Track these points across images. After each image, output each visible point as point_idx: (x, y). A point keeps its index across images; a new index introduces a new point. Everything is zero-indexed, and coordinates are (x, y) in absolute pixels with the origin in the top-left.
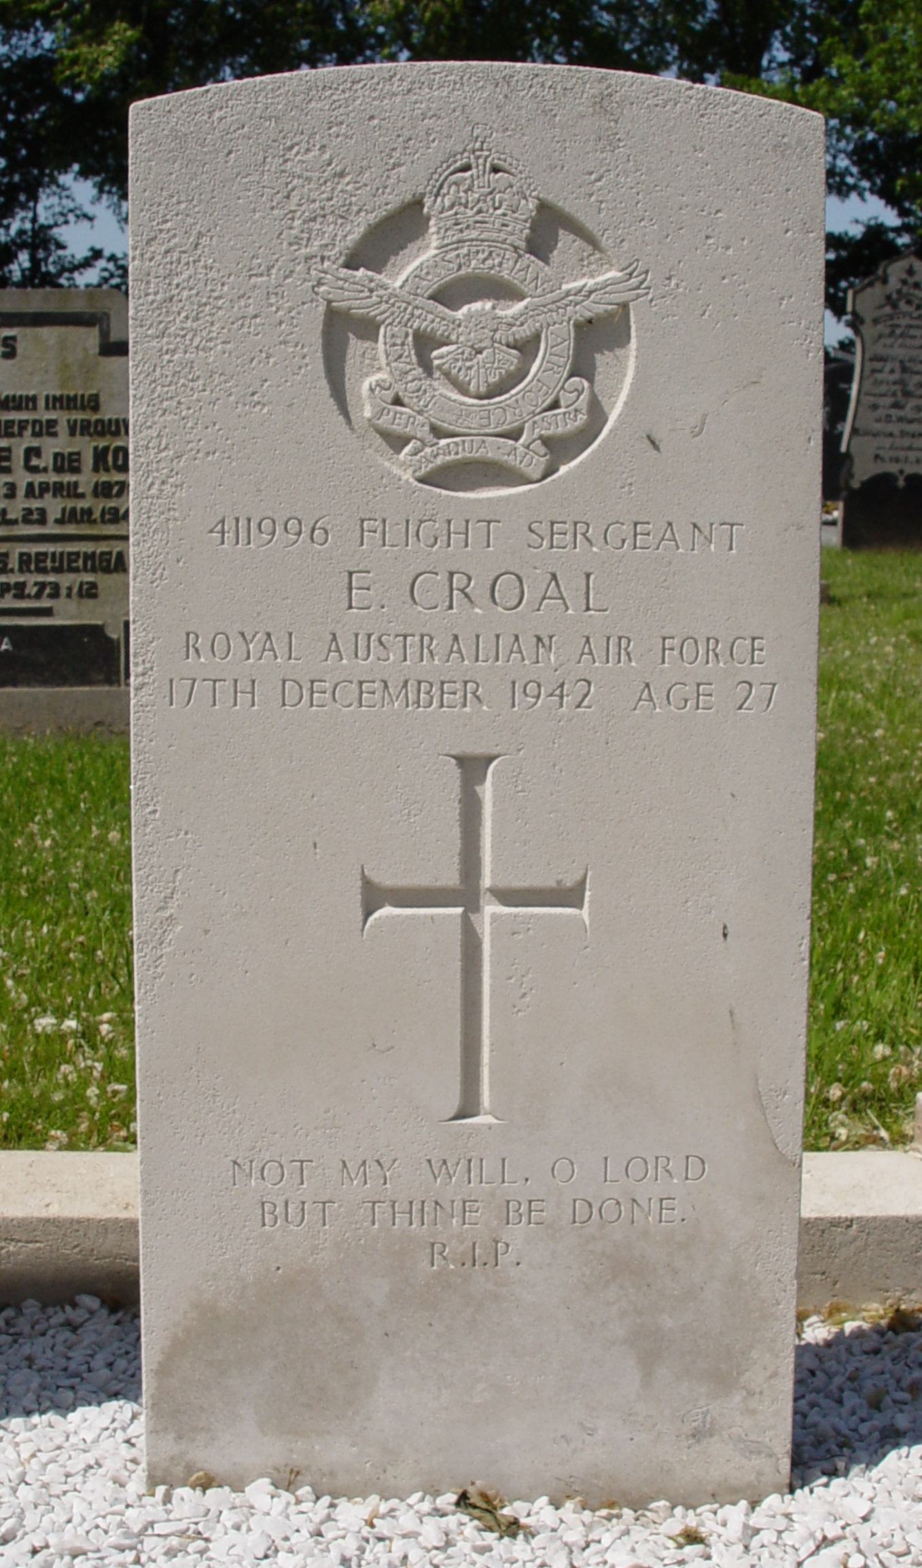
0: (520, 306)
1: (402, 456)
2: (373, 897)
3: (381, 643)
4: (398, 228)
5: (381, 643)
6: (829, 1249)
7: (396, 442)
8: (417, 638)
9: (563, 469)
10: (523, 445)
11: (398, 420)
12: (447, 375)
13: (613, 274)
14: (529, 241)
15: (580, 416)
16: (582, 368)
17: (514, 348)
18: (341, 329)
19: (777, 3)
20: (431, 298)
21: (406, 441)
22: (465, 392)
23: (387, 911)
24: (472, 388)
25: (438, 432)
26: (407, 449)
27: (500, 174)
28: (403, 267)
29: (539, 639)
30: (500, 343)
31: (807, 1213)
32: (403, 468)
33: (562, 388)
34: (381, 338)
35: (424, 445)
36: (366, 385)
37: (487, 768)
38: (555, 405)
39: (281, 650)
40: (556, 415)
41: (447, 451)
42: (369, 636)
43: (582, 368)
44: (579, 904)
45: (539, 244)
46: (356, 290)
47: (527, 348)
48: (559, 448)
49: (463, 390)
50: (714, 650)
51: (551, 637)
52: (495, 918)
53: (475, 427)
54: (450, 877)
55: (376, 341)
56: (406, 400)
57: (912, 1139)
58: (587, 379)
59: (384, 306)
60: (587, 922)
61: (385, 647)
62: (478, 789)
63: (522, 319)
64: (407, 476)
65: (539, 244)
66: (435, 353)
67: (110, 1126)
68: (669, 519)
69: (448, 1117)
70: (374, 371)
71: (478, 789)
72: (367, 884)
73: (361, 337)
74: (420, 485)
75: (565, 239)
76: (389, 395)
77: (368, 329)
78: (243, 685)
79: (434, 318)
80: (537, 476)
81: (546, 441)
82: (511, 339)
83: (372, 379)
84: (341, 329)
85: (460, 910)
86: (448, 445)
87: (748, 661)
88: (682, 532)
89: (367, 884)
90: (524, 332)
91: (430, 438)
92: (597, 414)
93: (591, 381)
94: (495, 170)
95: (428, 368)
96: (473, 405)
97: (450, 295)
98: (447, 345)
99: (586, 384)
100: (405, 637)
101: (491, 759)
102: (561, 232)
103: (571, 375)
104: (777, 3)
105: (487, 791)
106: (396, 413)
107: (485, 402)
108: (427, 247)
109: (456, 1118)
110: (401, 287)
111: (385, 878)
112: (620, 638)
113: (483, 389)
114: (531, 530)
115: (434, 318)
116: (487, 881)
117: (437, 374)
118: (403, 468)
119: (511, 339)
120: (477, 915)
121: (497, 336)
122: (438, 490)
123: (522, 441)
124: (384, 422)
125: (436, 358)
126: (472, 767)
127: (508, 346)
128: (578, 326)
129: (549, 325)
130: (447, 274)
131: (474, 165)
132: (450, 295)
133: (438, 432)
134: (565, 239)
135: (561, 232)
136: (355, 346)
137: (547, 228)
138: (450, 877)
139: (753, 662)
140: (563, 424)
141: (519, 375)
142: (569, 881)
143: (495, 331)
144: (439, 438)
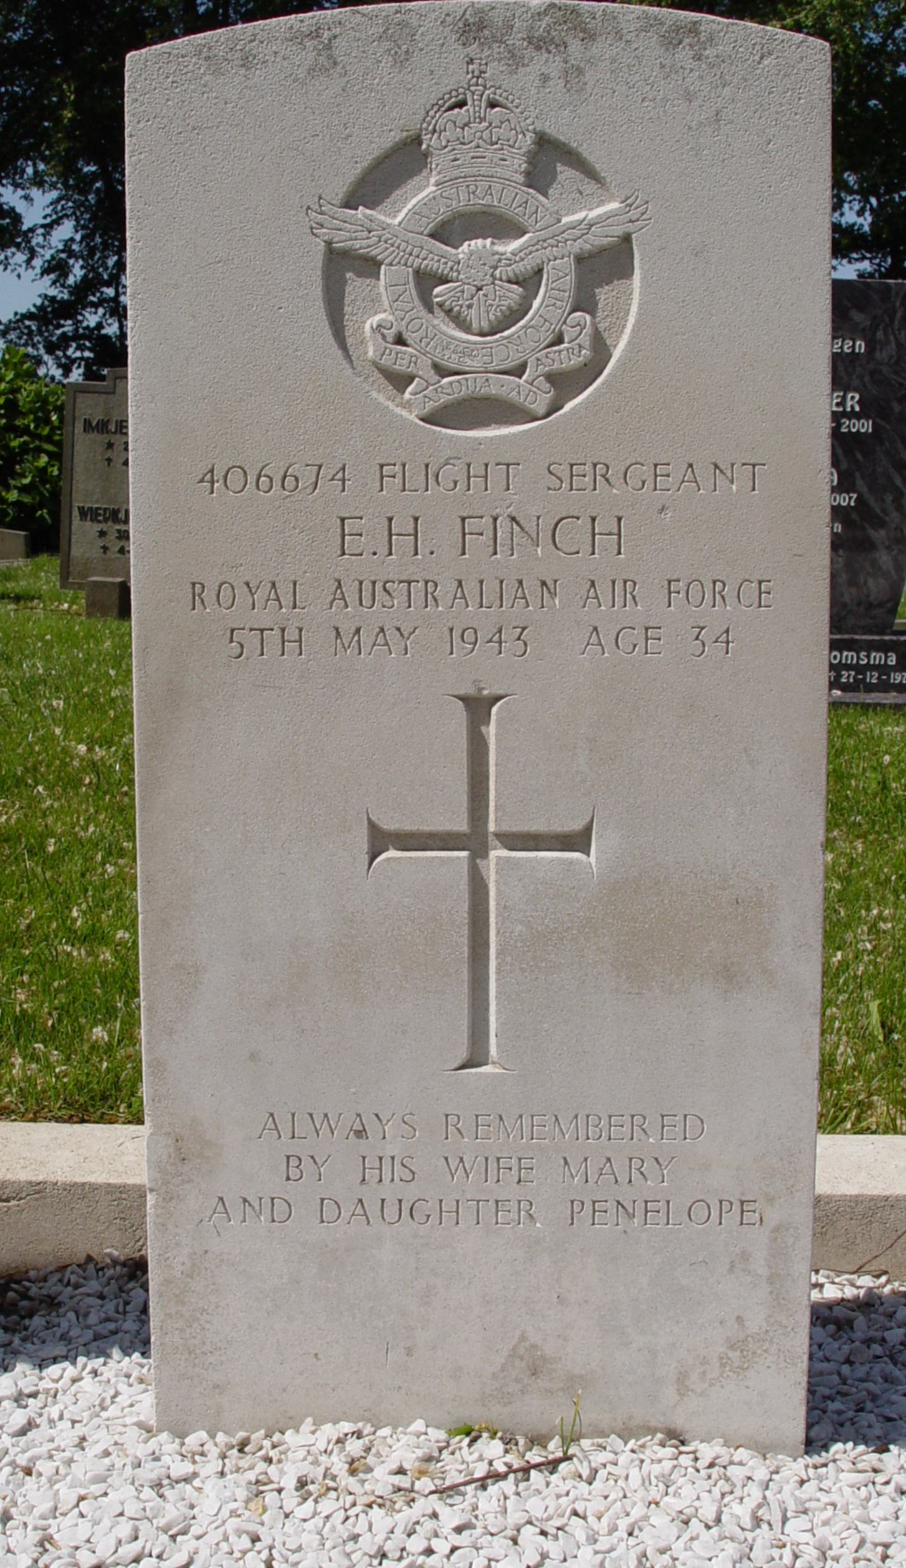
0: (515, 244)
1: (407, 395)
2: (380, 840)
3: (385, 589)
4: (403, 160)
5: (385, 589)
6: (838, 1223)
7: (400, 381)
8: (421, 584)
9: (568, 406)
10: (526, 381)
11: (401, 360)
12: (448, 312)
13: (614, 205)
14: (528, 174)
15: (584, 352)
16: (584, 302)
17: (516, 283)
18: (343, 265)
19: (3, 385)
20: (432, 235)
21: (410, 379)
22: (468, 329)
23: (392, 853)
24: (475, 325)
25: (442, 371)
26: (410, 389)
27: (497, 109)
28: (406, 201)
29: (544, 583)
30: (501, 280)
31: (823, 1188)
32: (407, 409)
33: (565, 322)
34: (382, 276)
35: (429, 384)
36: (367, 326)
37: (494, 704)
38: (559, 340)
39: (286, 600)
40: (560, 351)
41: (451, 389)
42: (374, 583)
43: (584, 302)
44: (587, 853)
45: (538, 177)
46: (356, 228)
47: (530, 281)
48: (565, 384)
49: (463, 325)
50: (720, 593)
51: (555, 581)
52: (499, 858)
53: (480, 363)
54: (461, 825)
55: (378, 279)
56: (410, 341)
57: (497, 835)
58: (588, 312)
59: (383, 245)
60: (594, 865)
61: (389, 594)
62: (483, 729)
63: (522, 254)
64: (412, 417)
65: (538, 177)
66: (437, 290)
67: (105, 1097)
68: (609, 1155)
69: (456, 1065)
70: (377, 308)
71: (483, 729)
72: (374, 829)
73: (359, 274)
74: (422, 423)
75: (565, 174)
76: (390, 334)
77: (370, 266)
78: (292, 634)
79: (437, 256)
80: (542, 411)
81: (550, 378)
82: (511, 274)
83: (375, 320)
84: (343, 265)
85: (464, 854)
86: (451, 383)
87: (756, 604)
88: (703, 472)
89: (374, 829)
90: (524, 267)
91: (432, 376)
92: (601, 350)
93: (592, 313)
94: (492, 105)
95: (429, 307)
96: (475, 343)
97: (449, 231)
98: (447, 282)
99: (588, 317)
100: (409, 583)
101: (498, 698)
102: (560, 167)
103: (574, 311)
104: (3, 385)
105: (491, 731)
106: (397, 353)
107: (489, 338)
108: (427, 186)
109: (463, 1067)
110: (400, 223)
111: (389, 824)
112: (625, 582)
113: (485, 325)
114: (550, 472)
115: (437, 256)
116: (492, 827)
117: (437, 310)
118: (407, 409)
119: (511, 274)
120: (485, 862)
121: (497, 272)
122: (438, 429)
123: (525, 377)
124: (385, 361)
125: (437, 296)
126: (478, 707)
127: (509, 281)
128: (580, 259)
129: (549, 260)
130: (442, 212)
131: (470, 103)
132: (449, 231)
133: (442, 371)
134: (565, 174)
135: (560, 167)
136: (355, 286)
137: (548, 158)
138: (461, 825)
139: (760, 606)
140: (568, 358)
141: (523, 309)
142: (577, 825)
143: (496, 268)
144: (443, 377)
